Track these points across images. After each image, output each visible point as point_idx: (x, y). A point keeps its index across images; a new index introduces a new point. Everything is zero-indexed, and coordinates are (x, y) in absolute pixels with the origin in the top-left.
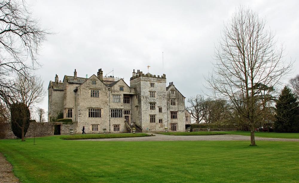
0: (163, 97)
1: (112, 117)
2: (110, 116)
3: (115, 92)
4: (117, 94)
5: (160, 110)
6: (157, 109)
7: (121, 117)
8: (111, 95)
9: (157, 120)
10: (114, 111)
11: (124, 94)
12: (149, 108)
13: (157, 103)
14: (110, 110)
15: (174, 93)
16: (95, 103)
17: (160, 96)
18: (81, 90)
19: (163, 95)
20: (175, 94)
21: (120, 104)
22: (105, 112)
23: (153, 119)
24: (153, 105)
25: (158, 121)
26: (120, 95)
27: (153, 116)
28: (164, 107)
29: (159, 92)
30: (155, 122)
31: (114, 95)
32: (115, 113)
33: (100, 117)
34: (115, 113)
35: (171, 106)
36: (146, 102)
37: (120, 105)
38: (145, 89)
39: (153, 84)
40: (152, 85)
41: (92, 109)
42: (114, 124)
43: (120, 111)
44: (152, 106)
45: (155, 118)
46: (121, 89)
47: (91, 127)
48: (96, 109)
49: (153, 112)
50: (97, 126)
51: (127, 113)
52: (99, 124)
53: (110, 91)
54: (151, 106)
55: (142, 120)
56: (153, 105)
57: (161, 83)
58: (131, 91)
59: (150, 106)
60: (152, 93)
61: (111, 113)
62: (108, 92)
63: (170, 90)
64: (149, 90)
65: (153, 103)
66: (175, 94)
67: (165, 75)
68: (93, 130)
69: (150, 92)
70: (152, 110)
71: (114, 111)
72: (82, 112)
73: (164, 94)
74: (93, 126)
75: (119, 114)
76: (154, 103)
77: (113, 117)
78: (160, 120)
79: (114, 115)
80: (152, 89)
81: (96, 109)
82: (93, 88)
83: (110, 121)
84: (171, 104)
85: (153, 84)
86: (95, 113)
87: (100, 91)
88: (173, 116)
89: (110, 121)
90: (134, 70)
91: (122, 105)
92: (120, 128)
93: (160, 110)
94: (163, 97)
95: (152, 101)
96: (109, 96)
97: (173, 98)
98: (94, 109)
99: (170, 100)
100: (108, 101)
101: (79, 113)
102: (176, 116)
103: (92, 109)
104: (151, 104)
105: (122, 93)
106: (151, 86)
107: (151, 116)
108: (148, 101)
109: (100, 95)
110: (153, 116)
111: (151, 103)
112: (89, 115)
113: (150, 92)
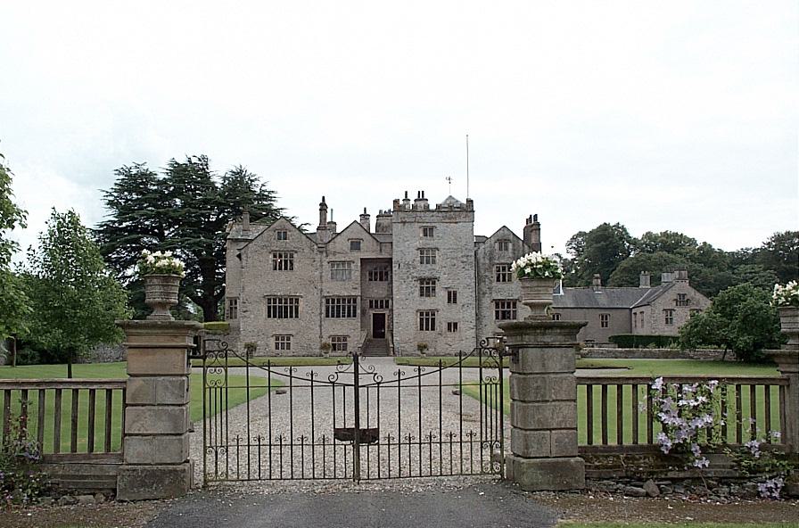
0: (463, 262)
1: (327, 316)
2: (321, 314)
3: (338, 255)
4: (343, 259)
5: (452, 297)
6: (441, 295)
7: (355, 316)
8: (325, 263)
9: (441, 324)
10: (333, 302)
11: (361, 259)
12: (417, 293)
13: (443, 277)
14: (324, 300)
15: (507, 249)
16: (282, 284)
17: (453, 258)
18: (249, 255)
19: (462, 257)
20: (510, 250)
21: (349, 285)
22: (310, 306)
23: (427, 320)
24: (428, 283)
25: (445, 326)
26: (349, 263)
27: (427, 314)
28: (464, 288)
29: (449, 249)
30: (433, 329)
31: (332, 263)
32: (337, 307)
33: (297, 317)
34: (337, 307)
35: (495, 284)
36: (408, 278)
37: (349, 286)
38: (406, 246)
39: (432, 229)
40: (428, 231)
41: (275, 300)
42: (332, 333)
43: (349, 302)
44: (427, 286)
45: (433, 320)
46: (355, 245)
47: (272, 342)
48: (286, 299)
49: (428, 304)
50: (288, 339)
51: (382, 307)
52: (294, 333)
53: (325, 254)
54: (422, 288)
55: (395, 324)
56: (428, 283)
57: (456, 223)
58: (381, 250)
59: (418, 289)
60: (427, 255)
61: (419, 320)
62: (318, 258)
63: (493, 242)
64: (418, 244)
65: (429, 279)
66: (510, 250)
67: (470, 202)
68: (277, 348)
69: (421, 250)
70: (427, 299)
71: (333, 302)
72: (250, 308)
73: (465, 253)
74: (277, 339)
75: (349, 307)
76: (433, 280)
77: (425, 331)
78: (449, 324)
79: (333, 311)
80: (431, 243)
81: (286, 299)
82: (277, 249)
83: (321, 326)
84: (498, 280)
85: (432, 229)
86: (282, 308)
87: (295, 255)
88: (504, 312)
89: (321, 326)
90: (406, 192)
91: (357, 286)
92: (349, 344)
93: (452, 297)
94: (463, 262)
95: (427, 274)
96: (322, 266)
97: (503, 261)
98: (344, 300)
99: (494, 269)
100: (317, 278)
101: (245, 309)
102: (515, 312)
103: (275, 300)
104: (422, 283)
105: (357, 256)
106: (425, 235)
107: (422, 314)
108: (415, 274)
109: (296, 265)
110: (427, 314)
111: (422, 280)
112: (269, 312)
113: (421, 250)
